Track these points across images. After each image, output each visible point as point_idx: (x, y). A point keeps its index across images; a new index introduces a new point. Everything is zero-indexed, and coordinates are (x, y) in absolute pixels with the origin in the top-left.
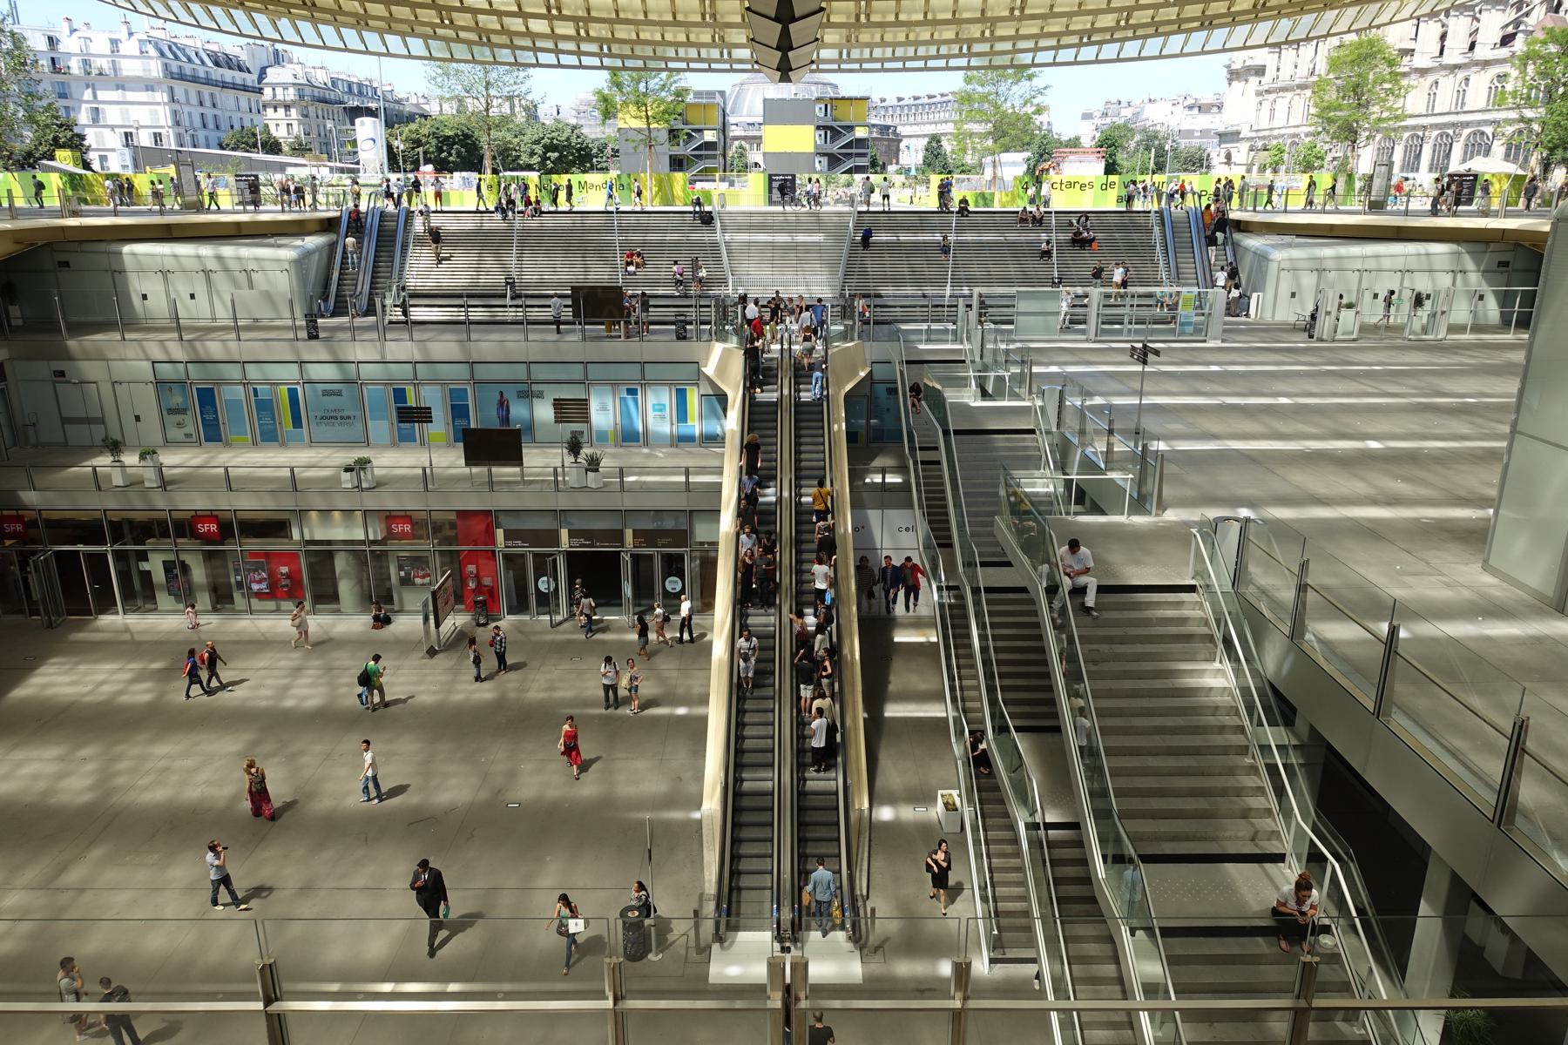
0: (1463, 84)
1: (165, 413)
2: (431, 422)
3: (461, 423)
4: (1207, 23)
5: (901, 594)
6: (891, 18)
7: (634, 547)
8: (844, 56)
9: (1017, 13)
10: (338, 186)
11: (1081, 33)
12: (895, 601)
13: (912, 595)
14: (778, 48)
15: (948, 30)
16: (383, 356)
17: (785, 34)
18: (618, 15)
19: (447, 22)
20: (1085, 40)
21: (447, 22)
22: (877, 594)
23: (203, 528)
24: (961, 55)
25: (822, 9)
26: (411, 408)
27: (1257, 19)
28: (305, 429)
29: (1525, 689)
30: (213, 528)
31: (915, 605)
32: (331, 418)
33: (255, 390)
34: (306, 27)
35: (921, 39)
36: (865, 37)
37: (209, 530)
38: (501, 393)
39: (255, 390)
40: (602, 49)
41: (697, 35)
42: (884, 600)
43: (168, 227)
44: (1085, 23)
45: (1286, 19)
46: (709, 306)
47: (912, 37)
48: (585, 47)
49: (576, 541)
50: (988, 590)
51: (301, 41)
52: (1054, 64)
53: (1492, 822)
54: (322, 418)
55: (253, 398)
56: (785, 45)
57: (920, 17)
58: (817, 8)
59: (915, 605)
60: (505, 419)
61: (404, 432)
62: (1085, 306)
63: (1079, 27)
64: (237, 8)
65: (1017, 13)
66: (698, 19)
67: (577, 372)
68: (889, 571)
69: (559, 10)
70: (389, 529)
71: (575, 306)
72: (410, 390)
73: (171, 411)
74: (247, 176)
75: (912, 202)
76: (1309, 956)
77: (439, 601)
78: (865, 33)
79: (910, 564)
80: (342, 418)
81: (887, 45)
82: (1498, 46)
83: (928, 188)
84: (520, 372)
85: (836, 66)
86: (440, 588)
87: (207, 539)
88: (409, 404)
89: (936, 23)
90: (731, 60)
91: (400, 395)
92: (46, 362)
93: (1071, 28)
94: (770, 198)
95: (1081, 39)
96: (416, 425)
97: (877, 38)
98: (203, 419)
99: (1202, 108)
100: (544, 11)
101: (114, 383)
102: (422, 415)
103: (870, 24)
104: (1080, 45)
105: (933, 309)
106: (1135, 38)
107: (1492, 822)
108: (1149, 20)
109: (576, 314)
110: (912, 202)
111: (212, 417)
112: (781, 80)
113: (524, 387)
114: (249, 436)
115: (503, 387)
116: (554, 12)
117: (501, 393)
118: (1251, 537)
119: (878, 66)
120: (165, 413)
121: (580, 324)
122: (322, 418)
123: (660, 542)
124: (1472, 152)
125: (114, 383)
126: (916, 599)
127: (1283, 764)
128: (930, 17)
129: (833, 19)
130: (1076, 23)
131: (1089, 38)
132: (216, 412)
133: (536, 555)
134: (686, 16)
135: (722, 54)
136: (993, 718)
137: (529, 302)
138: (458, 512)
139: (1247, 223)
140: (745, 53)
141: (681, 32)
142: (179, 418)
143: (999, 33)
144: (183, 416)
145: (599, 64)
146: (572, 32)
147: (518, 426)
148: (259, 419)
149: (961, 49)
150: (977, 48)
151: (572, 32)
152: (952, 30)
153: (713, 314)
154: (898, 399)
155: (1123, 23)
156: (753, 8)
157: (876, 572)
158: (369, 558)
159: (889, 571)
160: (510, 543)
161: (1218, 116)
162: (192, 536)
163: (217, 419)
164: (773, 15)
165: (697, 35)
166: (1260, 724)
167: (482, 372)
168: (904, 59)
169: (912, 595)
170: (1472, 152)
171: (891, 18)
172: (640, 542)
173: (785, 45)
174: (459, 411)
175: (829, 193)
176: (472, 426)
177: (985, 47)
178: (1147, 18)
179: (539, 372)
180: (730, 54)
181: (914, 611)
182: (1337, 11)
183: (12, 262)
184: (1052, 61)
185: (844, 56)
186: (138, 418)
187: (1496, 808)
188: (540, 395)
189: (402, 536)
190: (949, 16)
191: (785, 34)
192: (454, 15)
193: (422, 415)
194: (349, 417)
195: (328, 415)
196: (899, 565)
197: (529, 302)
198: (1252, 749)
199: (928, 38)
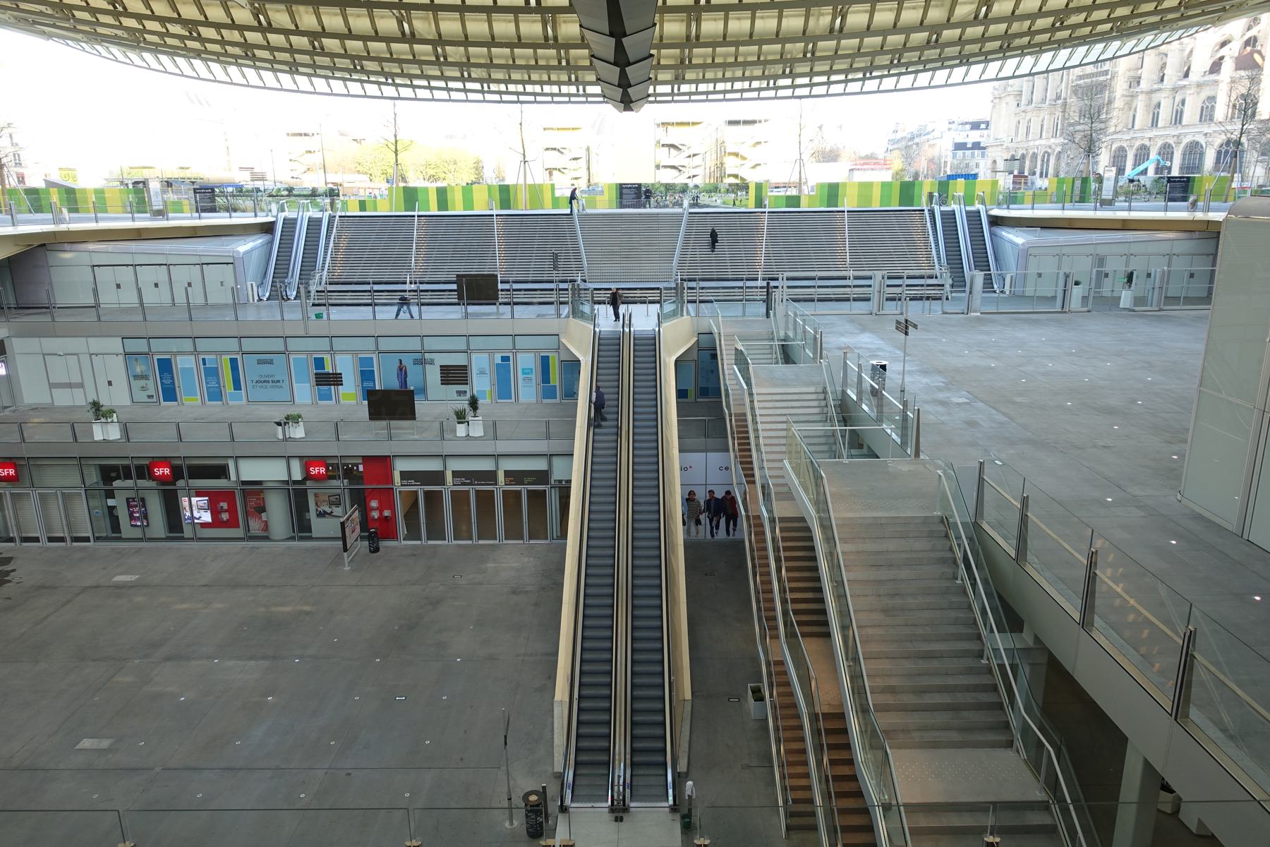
0: (1180, 105)
1: (131, 379)
2: (342, 385)
3: (368, 385)
4: (965, 61)
5: (723, 521)
6: (732, 60)
7: (506, 485)
8: (676, 91)
9: (809, 55)
10: (277, 196)
11: (864, 70)
12: (717, 527)
13: (732, 522)
14: (619, 86)
15: (757, 69)
16: (744, 306)
17: (623, 75)
18: (514, 62)
19: (359, 68)
20: (868, 75)
21: (359, 68)
22: (703, 522)
23: (159, 472)
24: (768, 88)
25: (652, 55)
26: (329, 374)
27: (1005, 58)
28: (243, 391)
29: (1191, 605)
30: (167, 471)
31: (734, 530)
32: (265, 381)
33: (204, 360)
34: (250, 73)
35: (754, 75)
36: (690, 75)
37: (163, 473)
38: (401, 361)
39: (204, 360)
40: (482, 87)
41: (752, 71)
42: (708, 527)
43: (139, 231)
44: (866, 62)
45: (1029, 57)
46: (567, 290)
47: (747, 74)
48: (469, 85)
49: (458, 480)
50: (782, 520)
51: (263, 85)
52: (810, 96)
53: (1171, 715)
54: (257, 382)
55: (202, 366)
56: (624, 83)
57: (755, 58)
58: (647, 55)
59: (734, 530)
60: (404, 382)
61: (322, 392)
62: (870, 286)
63: (862, 65)
64: (195, 58)
65: (809, 55)
66: (555, 63)
67: (460, 344)
68: (712, 503)
69: (445, 58)
70: (308, 471)
71: (460, 291)
72: (327, 358)
73: (136, 377)
74: (206, 192)
75: (734, 204)
76: (991, 837)
77: (347, 530)
78: (729, 70)
79: (729, 497)
80: (273, 382)
81: (708, 81)
82: (1207, 73)
83: (747, 193)
84: (414, 344)
85: (670, 98)
86: (348, 519)
87: (162, 480)
88: (326, 370)
89: (766, 63)
90: (586, 95)
91: (319, 363)
92: (37, 339)
93: (854, 66)
94: (621, 202)
95: (864, 75)
96: (332, 387)
97: (720, 75)
98: (162, 383)
99: (975, 126)
100: (434, 59)
101: (91, 355)
102: (336, 379)
103: (692, 66)
104: (864, 79)
105: (700, 291)
106: (925, 70)
107: (1171, 715)
108: (917, 59)
109: (460, 297)
110: (734, 204)
111: (169, 381)
112: (625, 110)
113: (418, 356)
114: (199, 397)
115: (401, 356)
116: (442, 59)
117: (401, 361)
118: (985, 477)
119: (721, 96)
120: (131, 379)
121: (464, 304)
122: (257, 382)
123: (526, 481)
124: (1144, 160)
125: (91, 355)
126: (735, 525)
127: (1009, 664)
128: (762, 58)
129: (662, 62)
130: (859, 62)
131: (871, 74)
132: (172, 378)
133: (427, 493)
134: (746, 57)
135: (578, 90)
136: (785, 625)
137: (376, 287)
138: (363, 457)
139: (1002, 218)
140: (597, 89)
141: (544, 73)
142: (142, 383)
143: (816, 69)
144: (147, 381)
145: (500, 99)
146: (458, 74)
147: (412, 388)
148: (207, 383)
149: (768, 84)
150: (781, 82)
151: (458, 74)
152: (760, 69)
153: (570, 296)
154: (717, 363)
155: (895, 62)
156: (596, 55)
157: (702, 503)
158: (297, 496)
159: (712, 503)
160: (405, 482)
161: (985, 132)
162: (150, 478)
163: (173, 383)
164: (612, 61)
165: (752, 71)
166: (992, 631)
167: (384, 344)
168: (759, 90)
169: (732, 522)
170: (1144, 160)
171: (709, 61)
172: (511, 481)
173: (624, 83)
174: (366, 375)
175: (667, 198)
176: (377, 388)
177: (788, 82)
178: (887, 60)
179: (430, 344)
180: (584, 90)
181: (734, 535)
182: (1070, 50)
183: (11, 263)
184: (877, 90)
185: (676, 91)
186: (110, 383)
187: (1173, 702)
188: (432, 362)
189: (318, 478)
190: (755, 58)
191: (623, 75)
192: (364, 62)
193: (336, 379)
194: (278, 381)
195: (262, 379)
196: (720, 497)
197: (376, 287)
198: (986, 652)
199: (741, 75)
